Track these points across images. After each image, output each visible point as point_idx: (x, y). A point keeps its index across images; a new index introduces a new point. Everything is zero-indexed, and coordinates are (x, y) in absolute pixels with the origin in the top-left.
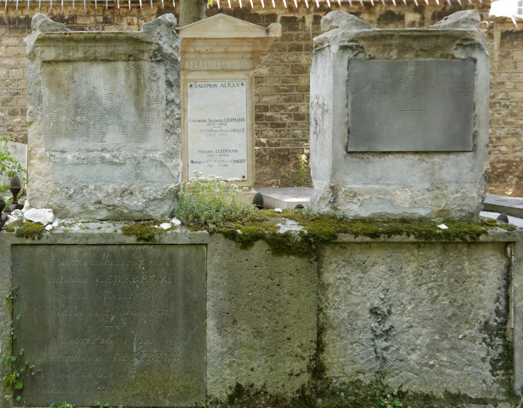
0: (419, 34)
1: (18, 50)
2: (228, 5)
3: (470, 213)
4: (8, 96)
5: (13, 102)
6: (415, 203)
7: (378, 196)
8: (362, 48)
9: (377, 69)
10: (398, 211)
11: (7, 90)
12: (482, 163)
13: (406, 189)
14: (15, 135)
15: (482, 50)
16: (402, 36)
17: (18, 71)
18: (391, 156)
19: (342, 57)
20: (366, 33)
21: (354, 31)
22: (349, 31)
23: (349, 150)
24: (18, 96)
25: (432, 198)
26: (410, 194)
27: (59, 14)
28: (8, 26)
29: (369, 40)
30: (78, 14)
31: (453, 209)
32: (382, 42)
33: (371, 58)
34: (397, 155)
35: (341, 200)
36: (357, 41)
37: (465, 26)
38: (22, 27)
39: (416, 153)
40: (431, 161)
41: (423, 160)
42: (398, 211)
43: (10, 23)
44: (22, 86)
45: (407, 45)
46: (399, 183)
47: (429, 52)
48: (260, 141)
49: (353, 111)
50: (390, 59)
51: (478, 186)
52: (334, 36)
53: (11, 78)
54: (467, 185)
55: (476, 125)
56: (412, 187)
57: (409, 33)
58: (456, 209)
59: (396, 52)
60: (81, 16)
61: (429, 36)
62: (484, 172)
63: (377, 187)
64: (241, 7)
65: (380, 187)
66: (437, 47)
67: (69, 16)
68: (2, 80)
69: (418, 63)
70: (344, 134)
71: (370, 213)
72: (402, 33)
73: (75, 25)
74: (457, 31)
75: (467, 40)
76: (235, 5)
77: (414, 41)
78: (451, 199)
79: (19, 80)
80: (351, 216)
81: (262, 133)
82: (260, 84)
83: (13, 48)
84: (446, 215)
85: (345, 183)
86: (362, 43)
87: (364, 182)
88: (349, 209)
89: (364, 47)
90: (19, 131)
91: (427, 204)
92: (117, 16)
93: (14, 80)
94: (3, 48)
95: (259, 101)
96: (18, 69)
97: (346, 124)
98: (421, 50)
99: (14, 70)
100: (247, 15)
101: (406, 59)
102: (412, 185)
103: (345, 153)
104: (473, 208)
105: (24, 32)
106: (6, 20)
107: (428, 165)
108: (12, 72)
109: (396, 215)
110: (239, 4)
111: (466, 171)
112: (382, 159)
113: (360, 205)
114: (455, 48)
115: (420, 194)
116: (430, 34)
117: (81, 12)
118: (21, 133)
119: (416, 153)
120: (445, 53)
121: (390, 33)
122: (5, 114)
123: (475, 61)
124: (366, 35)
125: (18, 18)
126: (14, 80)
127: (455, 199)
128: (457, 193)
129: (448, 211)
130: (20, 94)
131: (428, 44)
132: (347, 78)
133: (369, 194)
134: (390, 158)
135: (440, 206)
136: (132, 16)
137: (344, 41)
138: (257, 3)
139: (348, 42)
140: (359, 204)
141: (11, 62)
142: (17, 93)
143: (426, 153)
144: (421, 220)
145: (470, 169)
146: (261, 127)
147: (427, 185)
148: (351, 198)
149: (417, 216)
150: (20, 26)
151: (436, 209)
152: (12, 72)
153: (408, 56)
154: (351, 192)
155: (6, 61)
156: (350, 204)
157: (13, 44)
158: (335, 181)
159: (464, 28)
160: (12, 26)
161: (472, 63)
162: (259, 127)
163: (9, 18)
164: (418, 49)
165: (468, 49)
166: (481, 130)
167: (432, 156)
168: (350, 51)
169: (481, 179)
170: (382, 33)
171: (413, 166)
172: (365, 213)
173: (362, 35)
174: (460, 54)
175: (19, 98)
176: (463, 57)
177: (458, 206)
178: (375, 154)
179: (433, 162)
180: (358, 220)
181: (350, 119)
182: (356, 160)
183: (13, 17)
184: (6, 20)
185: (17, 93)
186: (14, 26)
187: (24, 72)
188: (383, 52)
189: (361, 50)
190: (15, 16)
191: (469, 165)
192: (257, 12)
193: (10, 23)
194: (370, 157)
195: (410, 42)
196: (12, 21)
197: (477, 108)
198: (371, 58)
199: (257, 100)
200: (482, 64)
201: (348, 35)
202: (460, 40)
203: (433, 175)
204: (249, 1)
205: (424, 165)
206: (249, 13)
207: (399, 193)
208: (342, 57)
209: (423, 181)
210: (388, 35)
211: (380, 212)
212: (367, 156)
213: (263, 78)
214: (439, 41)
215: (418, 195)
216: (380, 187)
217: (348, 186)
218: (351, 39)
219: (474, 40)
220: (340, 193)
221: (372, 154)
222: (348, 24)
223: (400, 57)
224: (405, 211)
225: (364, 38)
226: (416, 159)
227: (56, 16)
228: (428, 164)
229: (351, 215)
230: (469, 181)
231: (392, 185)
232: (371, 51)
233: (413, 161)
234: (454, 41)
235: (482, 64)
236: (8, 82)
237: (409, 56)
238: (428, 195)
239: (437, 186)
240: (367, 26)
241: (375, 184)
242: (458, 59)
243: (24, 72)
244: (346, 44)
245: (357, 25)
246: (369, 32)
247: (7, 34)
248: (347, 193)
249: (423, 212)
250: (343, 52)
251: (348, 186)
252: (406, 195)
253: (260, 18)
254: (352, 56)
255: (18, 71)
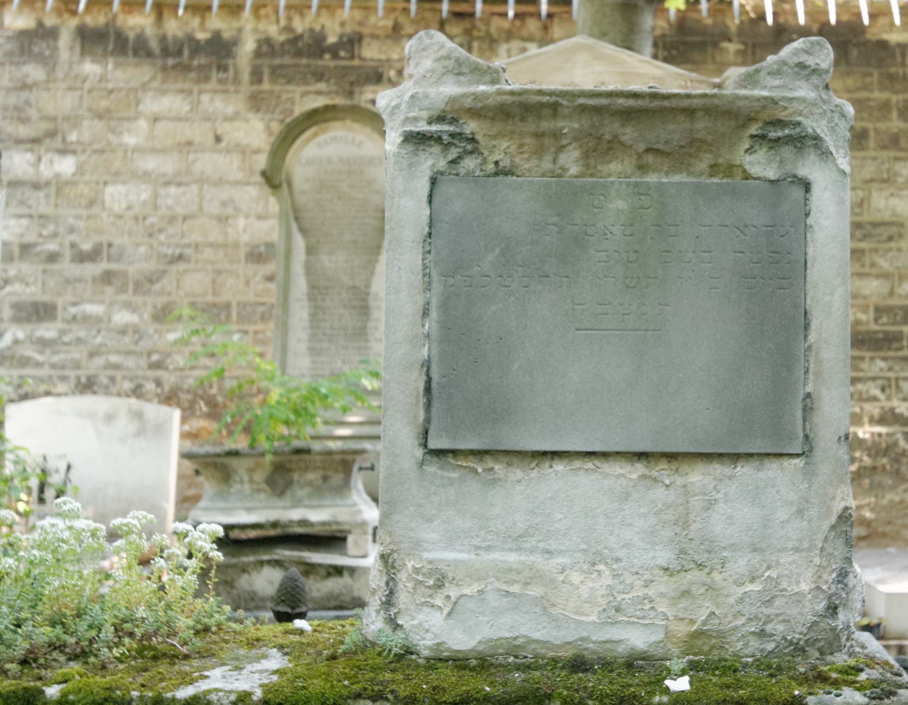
0: (631, 102)
1: (186, 131)
2: (795, 14)
3: (791, 643)
4: (152, 266)
5: (166, 283)
6: (618, 610)
7: (506, 588)
8: (473, 140)
9: (519, 200)
10: (562, 633)
11: (151, 246)
12: (830, 490)
13: (601, 567)
14: (169, 379)
15: (825, 154)
16: (583, 109)
17: (184, 194)
18: (559, 466)
19: (411, 165)
20: (476, 97)
21: (450, 89)
22: (432, 91)
23: (433, 444)
24: (182, 266)
25: (673, 595)
26: (609, 581)
27: (311, 30)
28: (159, 62)
29: (493, 119)
30: (366, 31)
31: (736, 628)
32: (531, 126)
33: (500, 172)
34: (577, 463)
35: (403, 598)
36: (454, 121)
37: (777, 82)
38: (200, 66)
39: (642, 456)
40: (680, 481)
41: (655, 480)
42: (562, 633)
43: (166, 51)
44: (196, 237)
45: (607, 137)
46: (583, 546)
47: (678, 156)
48: (892, 410)
49: (446, 326)
50: (560, 176)
51: (817, 560)
52: (394, 103)
53: (164, 211)
54: (785, 559)
55: (811, 377)
56: (618, 560)
57: (604, 101)
58: (745, 629)
59: (576, 154)
60: (374, 36)
61: (662, 111)
62: (833, 519)
63: (513, 558)
64: (833, 20)
65: (523, 558)
66: (695, 145)
67: (341, 36)
68: (136, 218)
69: (639, 190)
70: (417, 397)
71: (478, 638)
72: (582, 101)
73: (356, 62)
74: (746, 98)
75: (778, 123)
76: (816, 13)
77: (623, 126)
78: (731, 600)
79: (185, 218)
80: (426, 648)
81: (898, 387)
82: (893, 245)
83: (171, 125)
84: (713, 647)
85: (418, 545)
86: (470, 126)
87: (476, 542)
88: (420, 624)
89: (479, 137)
90: (181, 369)
91: (653, 614)
92: (479, 38)
93: (172, 219)
94: (143, 124)
95: (892, 293)
96: (187, 185)
97: (422, 366)
98: (649, 150)
99: (173, 190)
100: (855, 45)
101: (609, 175)
102: (621, 553)
103: (419, 453)
104: (799, 629)
105: (207, 79)
106: (154, 45)
107: (671, 496)
108: (168, 196)
109: (559, 647)
110: (826, 13)
111: (782, 514)
112: (534, 474)
113: (449, 614)
114: (747, 146)
115: (639, 583)
116: (666, 103)
117: (375, 26)
118: (188, 373)
119: (642, 456)
120: (721, 160)
121: (546, 99)
122: (141, 317)
123: (807, 186)
124: (480, 105)
125: (191, 39)
126: (172, 219)
127: (741, 600)
128: (753, 580)
129: (721, 635)
130: (188, 260)
131: (673, 132)
132: (427, 229)
133: (479, 579)
134: (556, 472)
135: (692, 622)
136: (524, 39)
137: (416, 119)
138: (879, 13)
139: (430, 123)
140: (446, 610)
141: (167, 165)
142: (180, 258)
143: (671, 457)
144: (633, 663)
145: (795, 508)
146: (897, 368)
147: (664, 556)
148: (430, 592)
149: (621, 649)
150: (195, 63)
151: (682, 630)
152: (168, 196)
153: (614, 167)
154: (430, 573)
155: (151, 163)
156: (426, 609)
157: (173, 114)
158: (388, 540)
159: (772, 88)
160: (170, 62)
161: (797, 193)
162: (890, 369)
163: (163, 39)
164: (641, 147)
165: (787, 151)
166: (824, 392)
167: (685, 468)
168: (436, 149)
169: (826, 539)
170: (522, 98)
171: (625, 497)
172: (462, 640)
173: (468, 102)
174: (761, 165)
175: (186, 271)
176: (771, 174)
177: (750, 620)
178: (515, 460)
179: (684, 486)
180: (446, 660)
181: (434, 352)
182: (455, 475)
183: (175, 37)
184: (154, 45)
185: (180, 258)
186: (177, 60)
187: (201, 197)
188: (539, 152)
189: (469, 147)
190: (180, 34)
191: (792, 496)
192: (885, 36)
193: (166, 51)
194: (497, 467)
195: (611, 128)
196: (171, 48)
197: (814, 326)
198: (500, 172)
199: (886, 290)
200: (827, 195)
201: (426, 103)
202: (760, 124)
203: (686, 525)
204: (858, 7)
205: (659, 493)
206: (862, 39)
207: (575, 578)
208: (411, 165)
209: (655, 544)
210: (542, 105)
211: (507, 635)
212: (490, 464)
213: (901, 225)
214: (701, 125)
215: (632, 586)
216: (523, 558)
217: (426, 555)
218: (436, 113)
219: (799, 124)
220: (402, 576)
221: (506, 459)
222: (433, 71)
223: (588, 169)
224: (585, 634)
225: (476, 113)
226: (634, 476)
227: (301, 36)
228: (671, 491)
229: (425, 644)
230: (790, 545)
231: (561, 553)
232: (501, 150)
233: (625, 483)
234: (744, 126)
235: (827, 195)
236: (153, 225)
237: (616, 168)
238: (664, 585)
239: (694, 558)
240: (487, 78)
241: (510, 550)
242: (758, 178)
243: (201, 197)
244: (423, 127)
245: (460, 74)
246: (485, 95)
247: (155, 84)
248: (420, 578)
249: (637, 639)
250: (415, 153)
251: (426, 555)
252: (598, 585)
253: (893, 56)
254: (442, 164)
255: (184, 194)
